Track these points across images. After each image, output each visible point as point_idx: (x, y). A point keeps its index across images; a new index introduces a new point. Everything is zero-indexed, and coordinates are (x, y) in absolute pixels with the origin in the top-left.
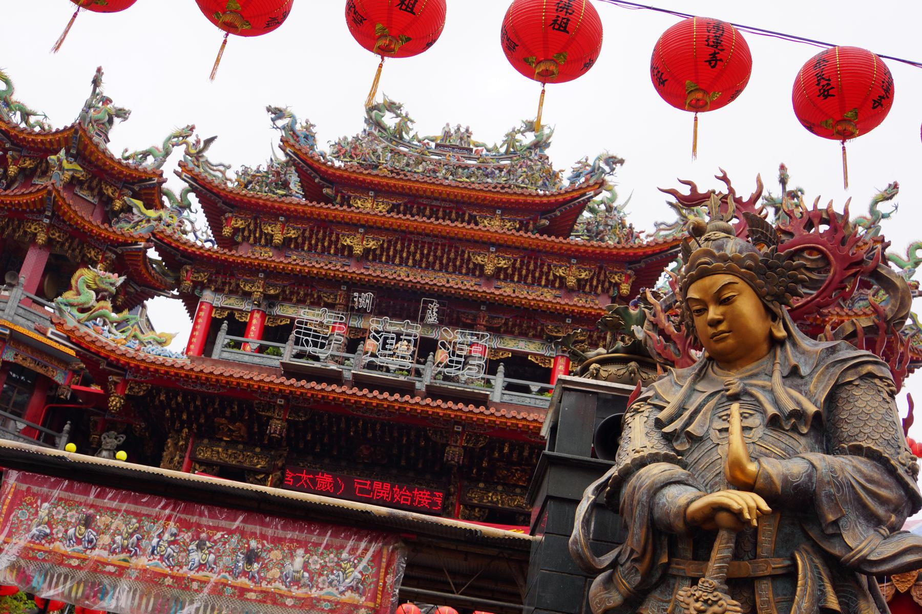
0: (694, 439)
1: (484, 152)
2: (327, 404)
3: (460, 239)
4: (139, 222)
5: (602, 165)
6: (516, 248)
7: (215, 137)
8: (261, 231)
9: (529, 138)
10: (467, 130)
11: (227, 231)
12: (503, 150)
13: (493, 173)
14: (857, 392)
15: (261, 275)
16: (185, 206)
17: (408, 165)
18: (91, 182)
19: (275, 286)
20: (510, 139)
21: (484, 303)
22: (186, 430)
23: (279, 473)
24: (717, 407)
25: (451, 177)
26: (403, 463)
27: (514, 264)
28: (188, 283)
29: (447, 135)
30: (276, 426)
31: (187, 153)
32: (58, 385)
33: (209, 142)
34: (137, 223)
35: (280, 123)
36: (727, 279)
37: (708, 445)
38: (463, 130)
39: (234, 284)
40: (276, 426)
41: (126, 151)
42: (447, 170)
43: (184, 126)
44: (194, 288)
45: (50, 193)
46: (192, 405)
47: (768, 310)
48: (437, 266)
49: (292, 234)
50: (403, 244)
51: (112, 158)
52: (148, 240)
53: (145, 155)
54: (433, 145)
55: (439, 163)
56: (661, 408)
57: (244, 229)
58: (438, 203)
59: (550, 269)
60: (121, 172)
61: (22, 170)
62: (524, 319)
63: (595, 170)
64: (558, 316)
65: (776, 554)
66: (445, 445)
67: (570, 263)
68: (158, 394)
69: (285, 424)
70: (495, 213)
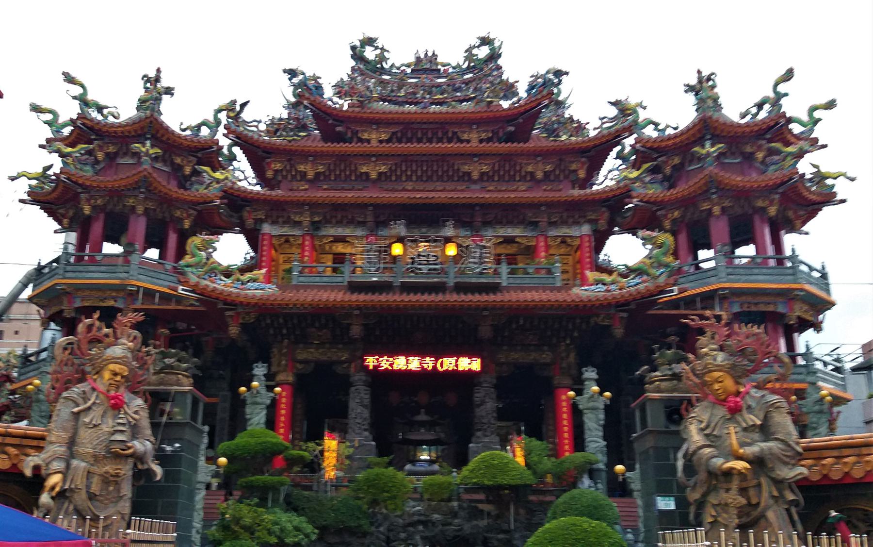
4: (209, 184)
5: (551, 76)
6: (494, 155)
7: (248, 102)
9: (483, 52)
11: (269, 174)
13: (460, 87)
14: (774, 414)
16: (232, 158)
17: (392, 91)
21: (477, 204)
24: (723, 423)
25: (428, 96)
27: (493, 168)
29: (418, 59)
30: (356, 331)
31: (228, 117)
34: (209, 185)
36: (721, 374)
38: (430, 54)
40: (356, 331)
41: (182, 124)
43: (228, 101)
44: (255, 223)
45: (145, 176)
49: (321, 169)
51: (167, 129)
52: (221, 198)
53: (199, 127)
54: (409, 70)
55: (416, 85)
62: (509, 213)
63: (547, 83)
64: (535, 206)
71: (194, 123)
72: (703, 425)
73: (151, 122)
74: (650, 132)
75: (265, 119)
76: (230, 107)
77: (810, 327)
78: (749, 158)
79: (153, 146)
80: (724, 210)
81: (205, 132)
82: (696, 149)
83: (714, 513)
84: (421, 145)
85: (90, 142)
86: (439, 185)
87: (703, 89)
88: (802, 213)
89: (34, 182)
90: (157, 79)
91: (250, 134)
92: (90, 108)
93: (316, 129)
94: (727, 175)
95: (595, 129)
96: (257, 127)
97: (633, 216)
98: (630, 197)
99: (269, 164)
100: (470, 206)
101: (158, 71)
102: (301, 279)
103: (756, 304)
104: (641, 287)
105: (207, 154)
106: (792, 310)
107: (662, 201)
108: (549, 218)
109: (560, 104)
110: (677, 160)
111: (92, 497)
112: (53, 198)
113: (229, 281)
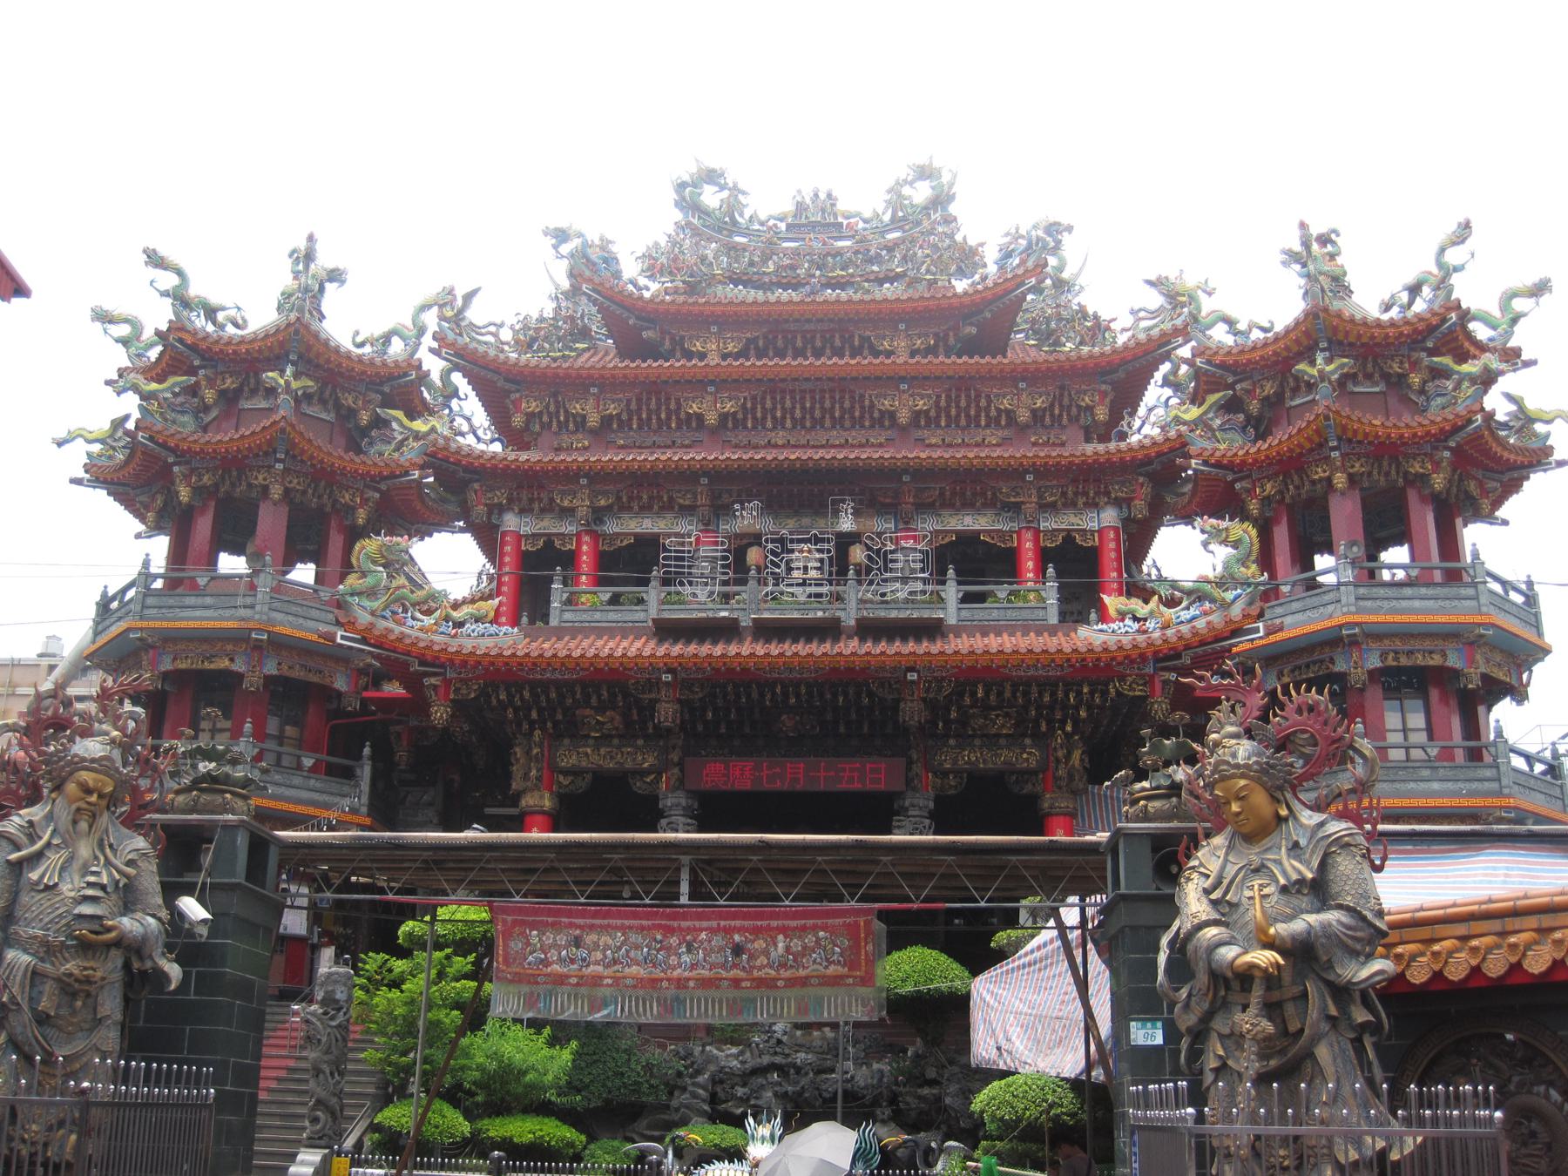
0: (1234, 906)
1: (861, 225)
2: (731, 671)
3: (855, 379)
8: (566, 411)
9: (921, 193)
10: (829, 196)
11: (518, 420)
12: (887, 218)
15: (584, 481)
17: (752, 264)
18: (322, 393)
19: (605, 494)
20: (896, 198)
21: (906, 471)
22: (537, 733)
23: (676, 770)
25: (818, 273)
26: (842, 729)
27: (937, 403)
28: (481, 509)
29: (801, 208)
30: (667, 713)
31: (442, 318)
32: (339, 694)
33: (468, 297)
34: (401, 443)
35: (565, 249)
37: (1242, 909)
38: (822, 196)
39: (545, 500)
40: (667, 713)
41: (357, 333)
42: (811, 262)
44: (490, 514)
45: (283, 431)
46: (543, 698)
47: (1272, 796)
48: (828, 423)
49: (612, 409)
50: (773, 398)
52: (422, 467)
53: (386, 339)
54: (783, 226)
55: (796, 253)
56: (1208, 876)
57: (541, 413)
58: (811, 327)
59: (989, 402)
60: (364, 373)
61: (222, 394)
64: (1014, 473)
65: (1294, 983)
66: (898, 701)
67: (1016, 387)
68: (496, 690)
69: (677, 706)
70: (896, 329)
71: (378, 331)
72: (1208, 884)
73: (297, 332)
74: (1220, 335)
75: (511, 320)
76: (444, 300)
77: (1505, 696)
78: (1397, 383)
79: (296, 376)
80: (1352, 480)
81: (397, 347)
82: (1301, 366)
83: (1221, 1053)
84: (765, 361)
85: (192, 371)
86: (836, 436)
87: (1315, 256)
88: (1491, 485)
89: (96, 448)
90: (309, 257)
91: (481, 349)
92: (192, 310)
93: (608, 337)
94: (1357, 414)
95: (1124, 330)
96: (495, 335)
97: (1194, 492)
98: (1188, 456)
99: (517, 403)
100: (889, 474)
101: (311, 238)
102: (568, 616)
103: (1410, 653)
104: (1201, 624)
105: (399, 388)
106: (1471, 661)
107: (1243, 462)
108: (1040, 497)
109: (1061, 285)
110: (1269, 389)
111: (42, 1019)
112: (138, 473)
113: (428, 621)
